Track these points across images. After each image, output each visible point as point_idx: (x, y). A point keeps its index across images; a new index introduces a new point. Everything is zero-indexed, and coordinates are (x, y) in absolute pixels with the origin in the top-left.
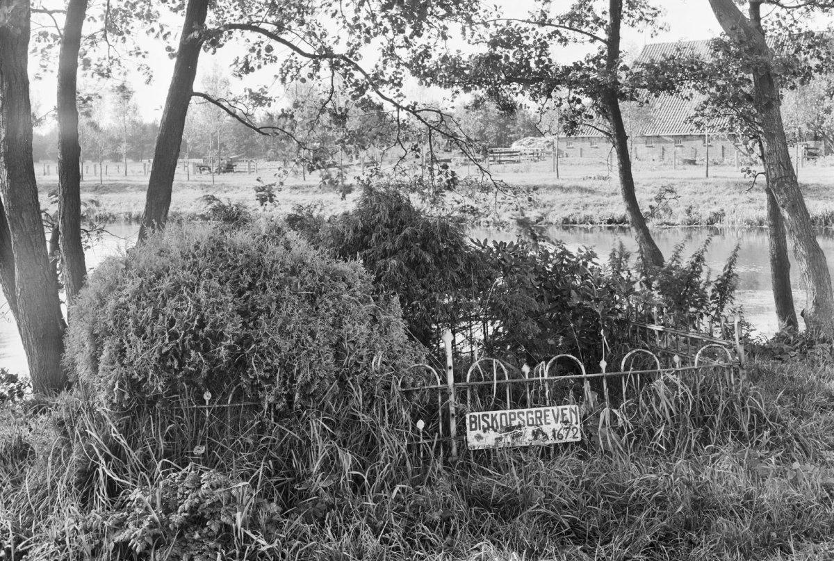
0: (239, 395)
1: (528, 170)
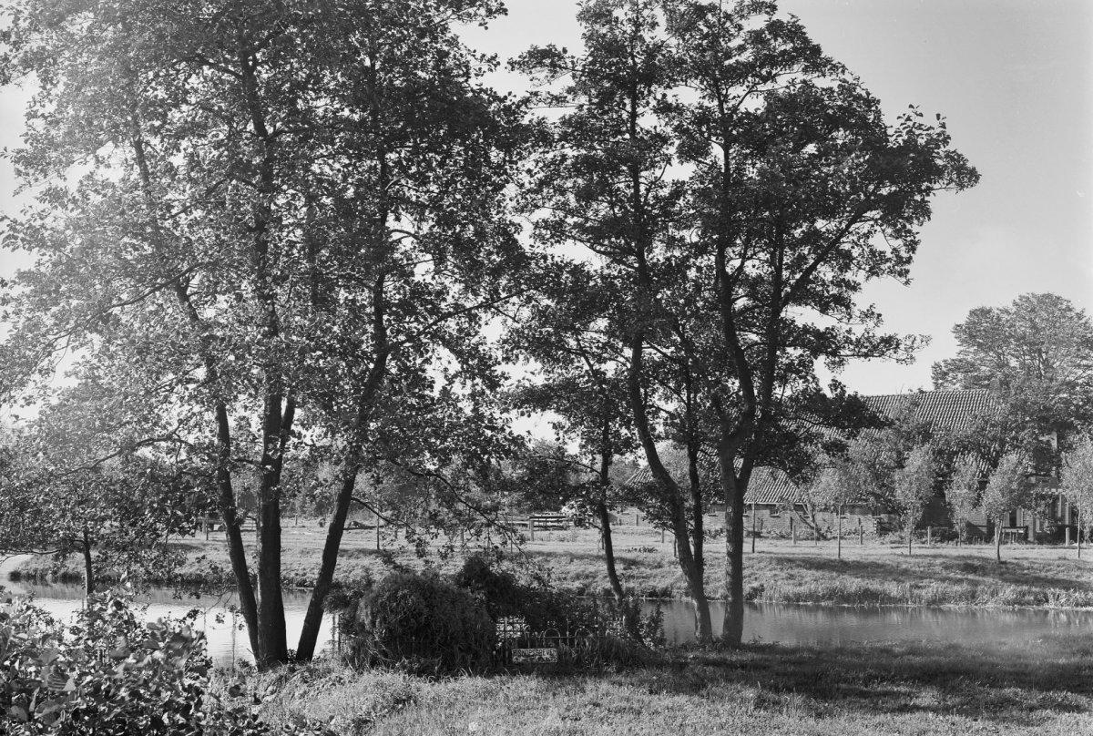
0: (426, 637)
1: (574, 539)
